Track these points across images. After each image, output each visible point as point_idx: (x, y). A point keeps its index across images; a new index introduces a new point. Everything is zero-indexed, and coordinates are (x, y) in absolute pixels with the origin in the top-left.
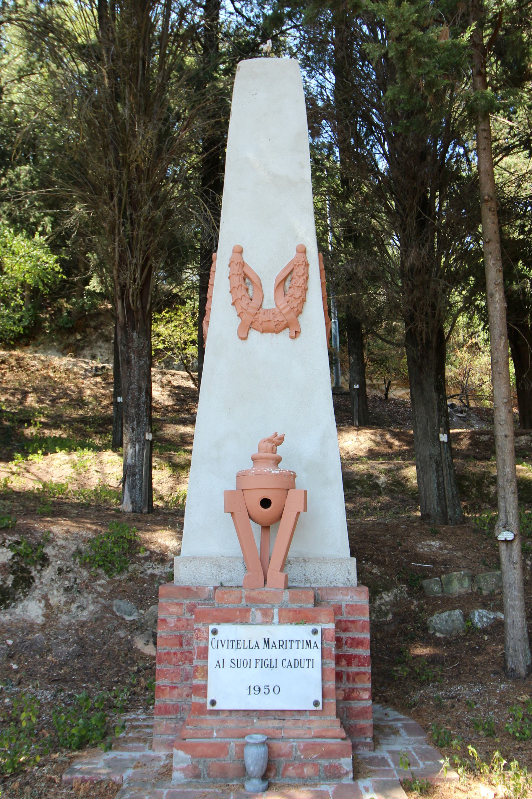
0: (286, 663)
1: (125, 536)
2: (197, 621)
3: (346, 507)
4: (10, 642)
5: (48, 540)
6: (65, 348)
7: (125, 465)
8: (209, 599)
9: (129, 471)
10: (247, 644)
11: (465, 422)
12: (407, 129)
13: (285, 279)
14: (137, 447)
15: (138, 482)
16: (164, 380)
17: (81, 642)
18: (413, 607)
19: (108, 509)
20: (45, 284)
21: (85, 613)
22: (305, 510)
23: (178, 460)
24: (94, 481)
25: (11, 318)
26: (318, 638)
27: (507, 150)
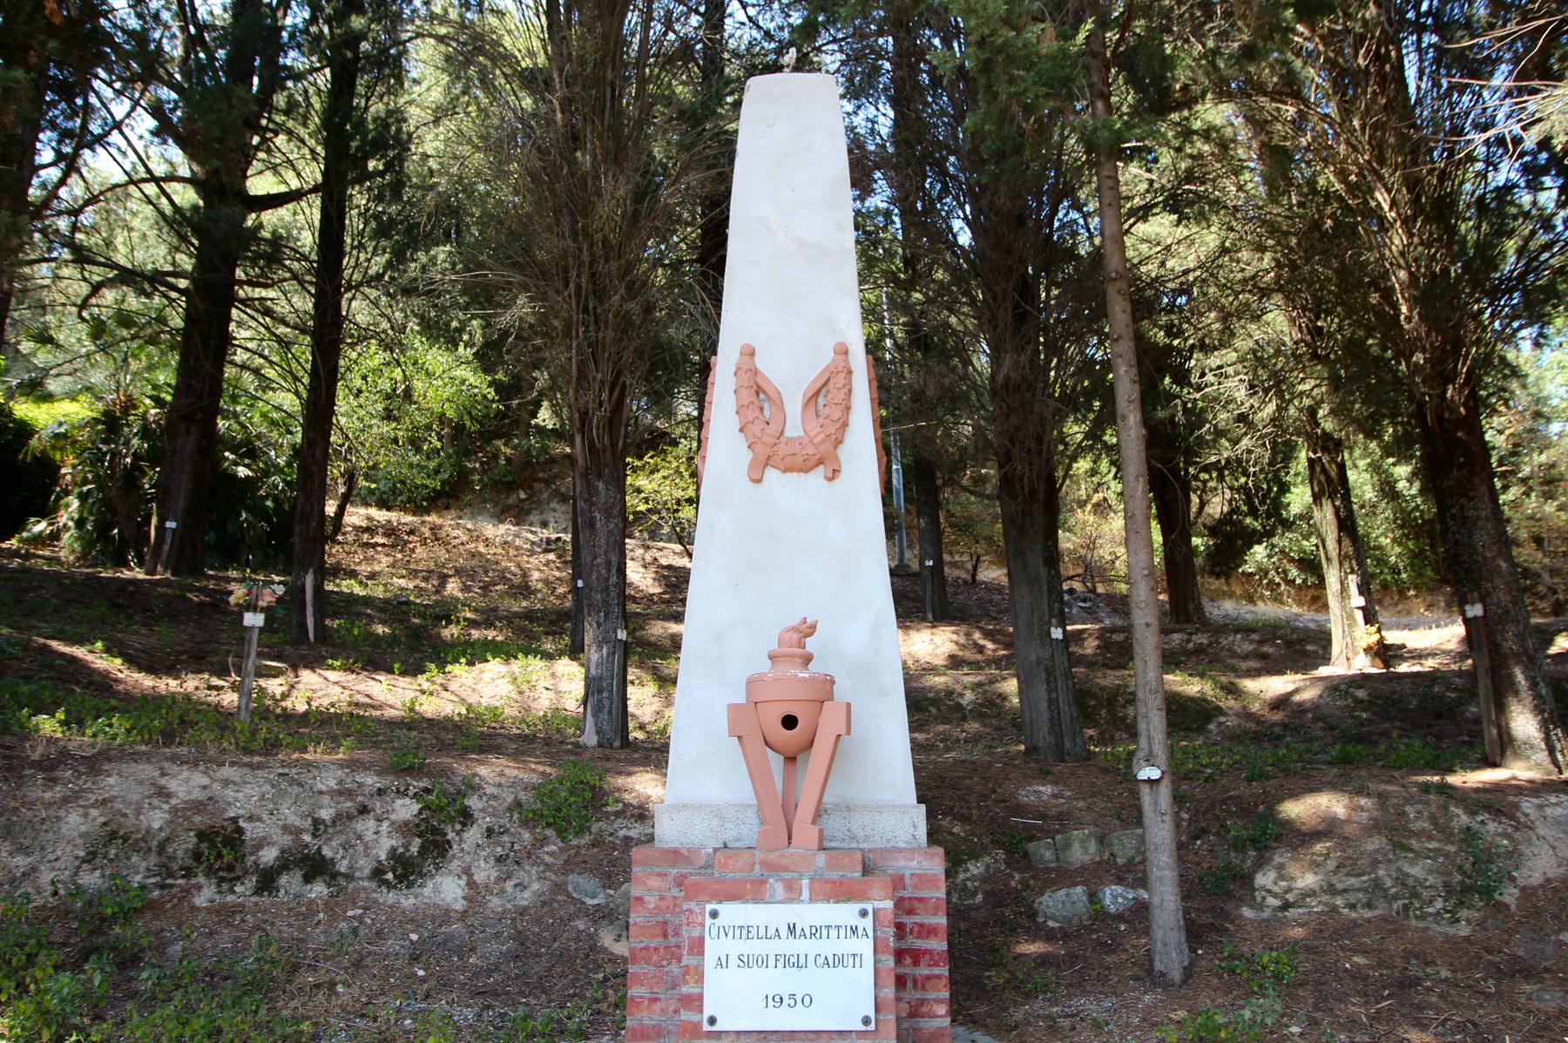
0: (820, 961)
1: (586, 783)
2: (687, 898)
3: (913, 741)
4: (414, 937)
5: (472, 786)
6: (503, 512)
7: (587, 678)
8: (706, 867)
9: (593, 687)
10: (762, 932)
11: (1090, 614)
12: (996, 178)
13: (817, 393)
14: (605, 650)
15: (606, 702)
16: (648, 558)
17: (520, 938)
18: (1013, 884)
19: (562, 743)
20: (472, 418)
21: (527, 894)
22: (848, 732)
23: (667, 671)
24: (543, 703)
25: (423, 468)
26: (868, 922)
27: (1144, 213)
